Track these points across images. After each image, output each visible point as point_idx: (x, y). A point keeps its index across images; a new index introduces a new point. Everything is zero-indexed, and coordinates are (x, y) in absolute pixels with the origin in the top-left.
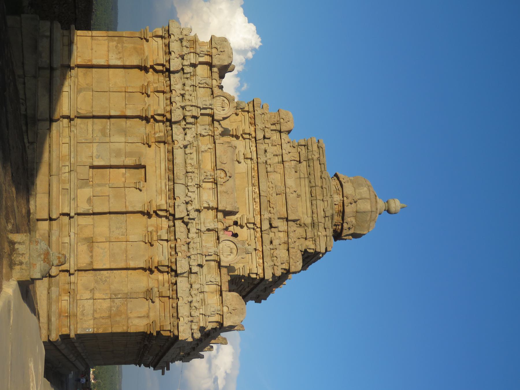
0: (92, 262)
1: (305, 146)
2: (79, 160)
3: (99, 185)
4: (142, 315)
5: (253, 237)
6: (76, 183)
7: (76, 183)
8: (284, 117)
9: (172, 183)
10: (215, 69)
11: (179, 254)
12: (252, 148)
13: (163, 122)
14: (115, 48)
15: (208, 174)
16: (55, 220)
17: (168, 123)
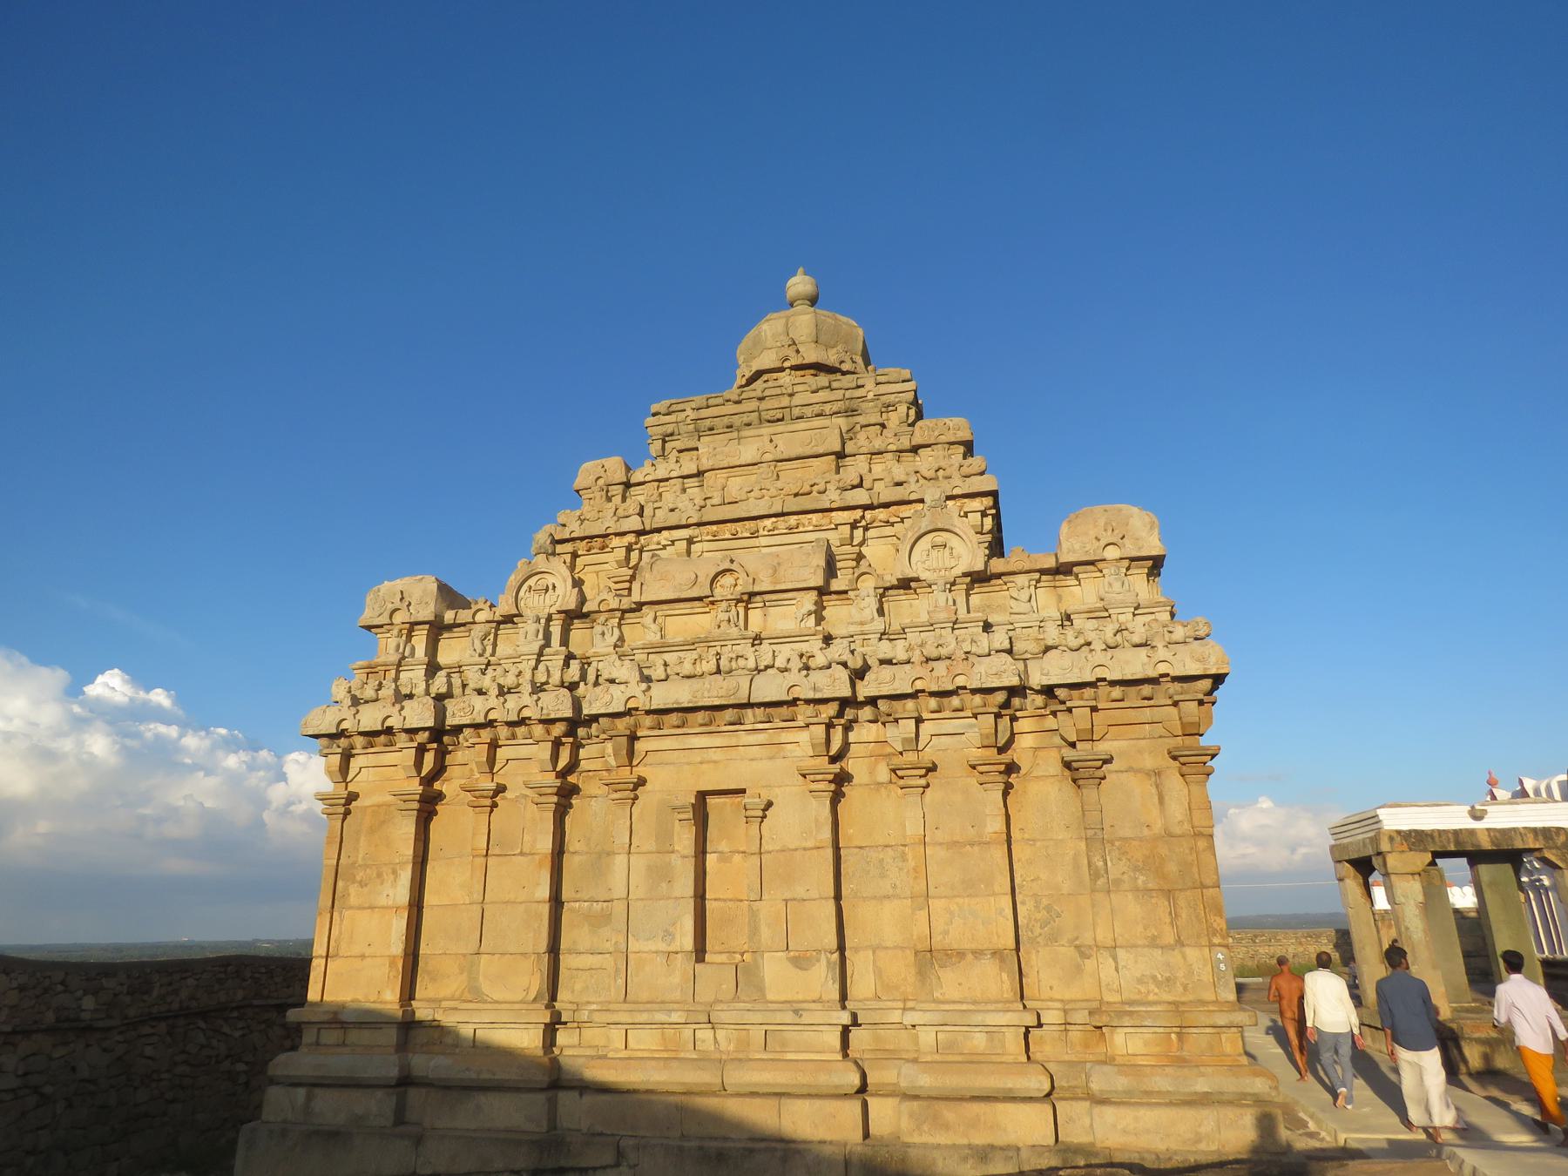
0: (994, 953)
1: (664, 442)
2: (677, 995)
3: (754, 931)
4: (1154, 790)
5: (888, 531)
6: (749, 1006)
7: (749, 1006)
8: (592, 478)
9: (749, 711)
10: (449, 616)
11: (960, 681)
12: (664, 542)
13: (577, 746)
14: (366, 890)
15: (724, 616)
16: (864, 1076)
17: (581, 732)
